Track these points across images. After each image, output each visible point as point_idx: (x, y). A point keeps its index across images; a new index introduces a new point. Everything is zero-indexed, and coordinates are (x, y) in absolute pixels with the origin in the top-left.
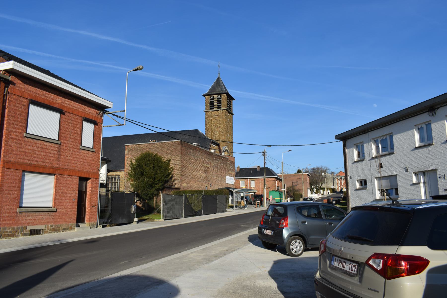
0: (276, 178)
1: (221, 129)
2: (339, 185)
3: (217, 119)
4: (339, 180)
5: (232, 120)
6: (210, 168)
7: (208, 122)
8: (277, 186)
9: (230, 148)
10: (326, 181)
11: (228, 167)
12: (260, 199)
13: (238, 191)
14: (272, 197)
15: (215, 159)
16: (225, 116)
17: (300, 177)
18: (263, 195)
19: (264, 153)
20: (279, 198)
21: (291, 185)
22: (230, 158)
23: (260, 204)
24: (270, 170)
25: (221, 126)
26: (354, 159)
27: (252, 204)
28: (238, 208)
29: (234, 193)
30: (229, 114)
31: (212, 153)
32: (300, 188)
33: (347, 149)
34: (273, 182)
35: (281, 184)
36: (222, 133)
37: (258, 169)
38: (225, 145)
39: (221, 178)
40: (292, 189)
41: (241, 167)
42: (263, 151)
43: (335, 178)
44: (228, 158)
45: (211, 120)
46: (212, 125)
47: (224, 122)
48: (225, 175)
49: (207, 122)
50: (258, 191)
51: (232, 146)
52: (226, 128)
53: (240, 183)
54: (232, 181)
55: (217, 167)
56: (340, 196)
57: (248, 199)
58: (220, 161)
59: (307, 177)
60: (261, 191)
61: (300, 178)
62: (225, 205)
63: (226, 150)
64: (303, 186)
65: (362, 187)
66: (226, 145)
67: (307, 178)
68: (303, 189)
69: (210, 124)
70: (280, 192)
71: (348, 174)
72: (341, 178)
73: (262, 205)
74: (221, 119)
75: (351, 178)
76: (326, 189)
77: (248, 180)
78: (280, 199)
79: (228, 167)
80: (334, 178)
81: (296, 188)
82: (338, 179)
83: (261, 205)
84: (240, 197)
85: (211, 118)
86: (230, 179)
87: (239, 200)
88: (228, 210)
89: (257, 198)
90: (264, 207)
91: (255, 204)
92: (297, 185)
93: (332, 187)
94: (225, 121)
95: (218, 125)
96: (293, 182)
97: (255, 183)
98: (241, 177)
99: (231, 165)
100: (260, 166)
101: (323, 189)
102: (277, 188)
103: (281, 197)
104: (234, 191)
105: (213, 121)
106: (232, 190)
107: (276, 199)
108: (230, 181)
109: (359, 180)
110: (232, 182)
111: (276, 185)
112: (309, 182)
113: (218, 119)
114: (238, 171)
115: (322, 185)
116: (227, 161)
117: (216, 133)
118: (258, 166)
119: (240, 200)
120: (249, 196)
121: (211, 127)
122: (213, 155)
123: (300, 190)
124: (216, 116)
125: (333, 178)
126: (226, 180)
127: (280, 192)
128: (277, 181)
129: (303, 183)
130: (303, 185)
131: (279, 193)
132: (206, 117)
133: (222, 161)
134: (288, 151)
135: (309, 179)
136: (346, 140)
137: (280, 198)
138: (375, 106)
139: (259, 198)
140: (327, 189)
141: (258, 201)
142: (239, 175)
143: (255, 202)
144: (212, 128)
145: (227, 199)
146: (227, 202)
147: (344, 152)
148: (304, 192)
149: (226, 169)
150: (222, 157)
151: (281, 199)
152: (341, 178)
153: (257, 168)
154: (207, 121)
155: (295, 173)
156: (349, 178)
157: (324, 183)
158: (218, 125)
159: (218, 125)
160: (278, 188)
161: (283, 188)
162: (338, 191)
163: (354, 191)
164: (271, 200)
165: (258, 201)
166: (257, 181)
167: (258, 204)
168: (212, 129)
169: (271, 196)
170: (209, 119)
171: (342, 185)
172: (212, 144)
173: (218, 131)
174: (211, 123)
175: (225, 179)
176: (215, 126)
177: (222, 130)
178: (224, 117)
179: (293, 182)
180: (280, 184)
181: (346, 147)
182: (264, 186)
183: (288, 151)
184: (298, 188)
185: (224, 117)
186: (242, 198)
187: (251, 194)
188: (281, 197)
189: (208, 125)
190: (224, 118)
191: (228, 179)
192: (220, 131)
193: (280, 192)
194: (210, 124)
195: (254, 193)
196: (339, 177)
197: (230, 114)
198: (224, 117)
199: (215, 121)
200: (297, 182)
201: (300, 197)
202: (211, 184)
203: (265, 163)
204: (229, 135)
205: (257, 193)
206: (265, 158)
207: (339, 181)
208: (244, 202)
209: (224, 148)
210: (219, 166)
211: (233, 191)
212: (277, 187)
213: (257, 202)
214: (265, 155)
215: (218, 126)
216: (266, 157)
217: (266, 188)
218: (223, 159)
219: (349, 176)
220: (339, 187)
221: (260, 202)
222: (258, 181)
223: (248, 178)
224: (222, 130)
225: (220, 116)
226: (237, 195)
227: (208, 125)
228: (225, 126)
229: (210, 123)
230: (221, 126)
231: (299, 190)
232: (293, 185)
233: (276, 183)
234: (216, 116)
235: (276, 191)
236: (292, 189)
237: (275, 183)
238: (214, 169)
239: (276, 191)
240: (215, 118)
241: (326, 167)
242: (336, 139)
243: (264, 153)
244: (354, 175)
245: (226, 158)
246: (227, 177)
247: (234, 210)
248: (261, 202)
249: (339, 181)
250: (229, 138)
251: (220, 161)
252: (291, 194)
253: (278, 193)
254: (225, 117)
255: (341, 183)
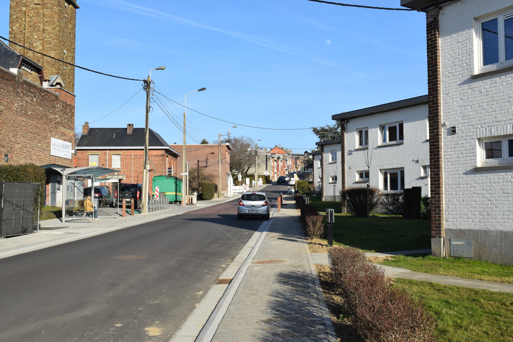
0: (167, 151)
1: (48, 36)
2: (275, 171)
3: (38, 12)
4: (275, 160)
5: (73, 18)
6: (7, 113)
7: (17, 18)
8: (167, 167)
9: (69, 80)
10: (257, 162)
11: (57, 116)
12: (132, 194)
13: (75, 173)
14: (158, 190)
15: (22, 92)
16: (58, 6)
17: (213, 152)
18: (142, 184)
19: (147, 83)
20: (174, 193)
21: (195, 167)
22: (62, 95)
23: (133, 207)
24: (154, 133)
25: (47, 28)
26: (472, 69)
27: (114, 205)
28: (74, 218)
29: (64, 177)
30: (66, 4)
31: (13, 76)
32: (214, 173)
33: (442, 37)
34: (161, 158)
35: (175, 163)
36: (50, 44)
37: (129, 132)
38: (56, 72)
39: (37, 141)
40: (196, 174)
41: (91, 126)
42: (146, 79)
43: (271, 158)
44: (57, 94)
45: (25, 12)
46: (25, 25)
47: (56, 20)
48: (49, 135)
49: (14, 17)
50: (127, 177)
51: (71, 77)
52: (58, 33)
53: (88, 159)
54: (68, 150)
55: (26, 114)
56: (287, 190)
57: (104, 194)
58: (35, 99)
59: (227, 151)
60: (134, 177)
61: (213, 153)
62: (30, 212)
63: (58, 84)
64: (220, 168)
65: (499, 163)
66: (58, 73)
67: (227, 153)
68: (220, 175)
69: (20, 21)
70: (177, 180)
71: (442, 119)
72: (279, 158)
73: (138, 207)
74: (49, 13)
75: (453, 131)
76: (256, 177)
77: (106, 154)
78: (176, 195)
79: (57, 116)
80: (268, 157)
81: (206, 172)
82: (275, 159)
83: (135, 209)
84: (82, 191)
85: (24, 9)
86: (61, 145)
87: (78, 196)
88: (43, 223)
89: (127, 191)
90: (142, 214)
91: (121, 206)
92: (206, 167)
93: (266, 173)
94: (58, 18)
95: (39, 25)
96: (198, 161)
97: (121, 160)
98: (91, 146)
99: (65, 113)
100: (133, 125)
101: (252, 177)
102: (167, 170)
103: (177, 189)
104: (66, 173)
105: (28, 16)
106: (59, 170)
107: (166, 193)
108: (60, 150)
109: (483, 138)
110: (66, 153)
111: (165, 165)
112: (229, 163)
113: (40, 11)
114: (86, 133)
115: (249, 168)
116: (53, 101)
117: (35, 44)
118: (130, 125)
119: (81, 197)
120: (107, 187)
121: (22, 29)
122: (14, 80)
123: (212, 176)
124: (36, 4)
125: (267, 157)
126: (52, 147)
127: (177, 180)
128: (167, 156)
129: (220, 164)
130: (220, 166)
131: (174, 181)
132: (12, 4)
133: (42, 100)
134: (199, 90)
135: (229, 155)
136: (441, 8)
137: (176, 192)
138: (329, 42)
139: (131, 193)
140: (259, 177)
141: (128, 200)
142: (86, 141)
143: (121, 201)
144: (27, 31)
145: (38, 194)
146: (37, 202)
147: (428, 46)
148: (220, 182)
149: (51, 120)
150: (42, 90)
151: (178, 194)
152: (279, 158)
153: (126, 129)
154: (13, 15)
155: (40, 226)
156: (443, 131)
157: (253, 165)
158: (39, 27)
159: (39, 25)
160: (171, 171)
161: (184, 172)
162: (273, 181)
163: (466, 174)
164: (155, 196)
165: (128, 200)
166: (126, 155)
167: (128, 207)
168: (27, 35)
169: (156, 188)
170: (19, 11)
171: (280, 170)
172: (23, 65)
173: (40, 40)
174: (24, 19)
175: (48, 144)
176: (34, 27)
177: (50, 37)
178: (56, 9)
179: (199, 160)
180: (174, 163)
181: (438, 31)
182: (145, 165)
183: (199, 90)
184: (208, 173)
185: (56, 9)
186: (87, 192)
187: (113, 183)
188: (177, 189)
189: (17, 25)
190: (56, 10)
191: (55, 145)
192: (46, 39)
193: (176, 179)
194: (20, 21)
195: (120, 180)
196: (276, 156)
197: (69, 4)
198: (55, 7)
199: (33, 16)
200: (207, 161)
201: (214, 190)
202: (6, 155)
203: (150, 107)
204: (65, 51)
205: (126, 181)
206: (150, 97)
207: (276, 163)
208: (92, 202)
209: (53, 78)
210: (33, 110)
211: (61, 172)
212: (168, 168)
213: (127, 202)
214: (149, 88)
215: (41, 29)
216: (151, 95)
217: (148, 167)
218: (43, 96)
219: (444, 125)
220: (275, 173)
221: (133, 201)
222: (128, 155)
223: (106, 150)
224: (50, 37)
225: (46, 7)
226: (74, 184)
227: (17, 25)
228: (58, 28)
229: (21, 19)
230: (47, 28)
231: (210, 177)
232: (198, 167)
233: (165, 160)
234: (36, 4)
235: (170, 176)
236: (196, 174)
237: (164, 161)
238: (19, 118)
239: (167, 178)
240: (33, 8)
241: (250, 139)
242: (401, 6)
243: (147, 84)
244: (466, 121)
245: (51, 94)
246: (53, 140)
247: (64, 224)
248: (136, 202)
249: (275, 162)
250: (67, 57)
251: (35, 99)
252: (195, 185)
253: (172, 181)
254: (59, 8)
255: (278, 166)
